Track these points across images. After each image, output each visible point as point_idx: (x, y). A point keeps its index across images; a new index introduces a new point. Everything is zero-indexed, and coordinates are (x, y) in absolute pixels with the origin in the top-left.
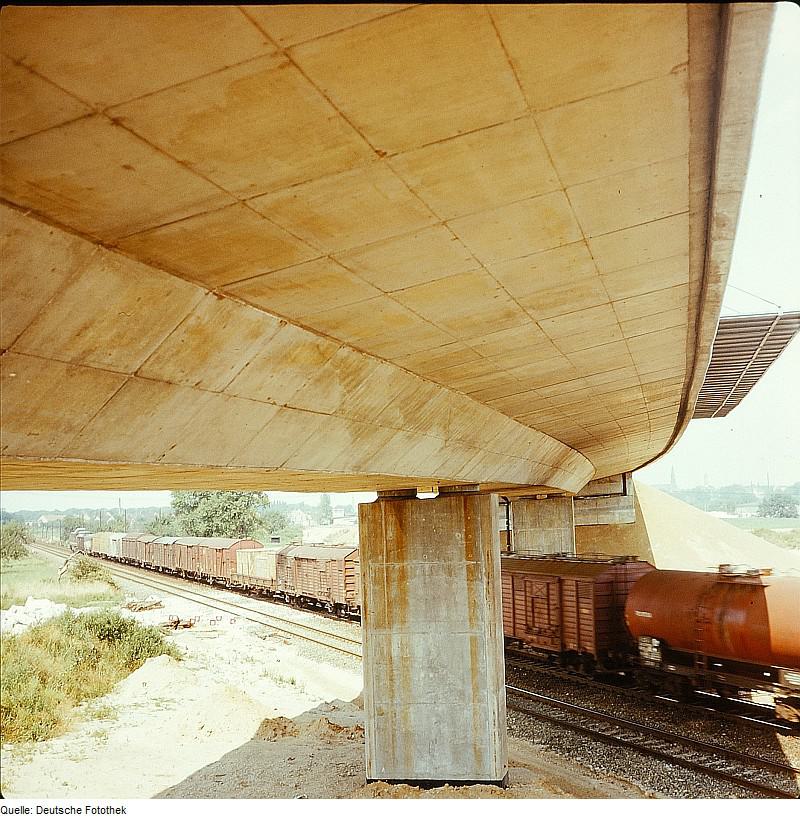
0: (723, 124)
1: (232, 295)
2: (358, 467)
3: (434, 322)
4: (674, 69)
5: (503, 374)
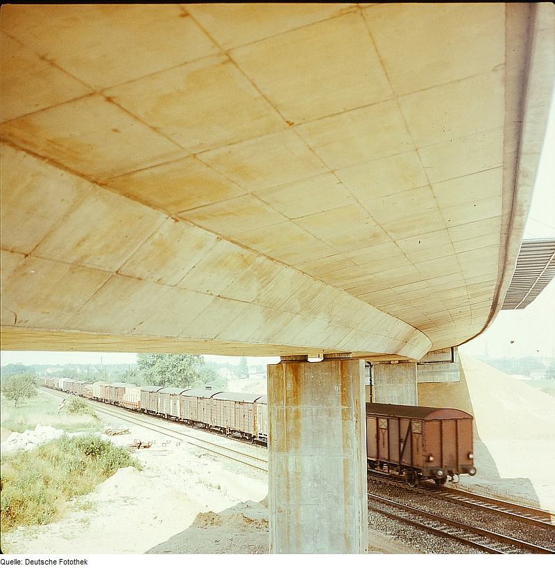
0: (529, 105)
3: (323, 240)
4: (497, 67)
5: (371, 277)
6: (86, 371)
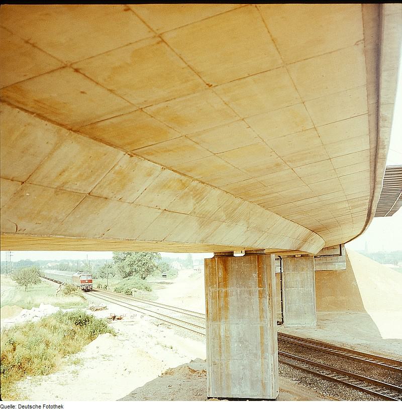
0: (382, 70)
1: (137, 155)
2: (202, 241)
3: (240, 168)
4: (357, 42)
6: (76, 265)
